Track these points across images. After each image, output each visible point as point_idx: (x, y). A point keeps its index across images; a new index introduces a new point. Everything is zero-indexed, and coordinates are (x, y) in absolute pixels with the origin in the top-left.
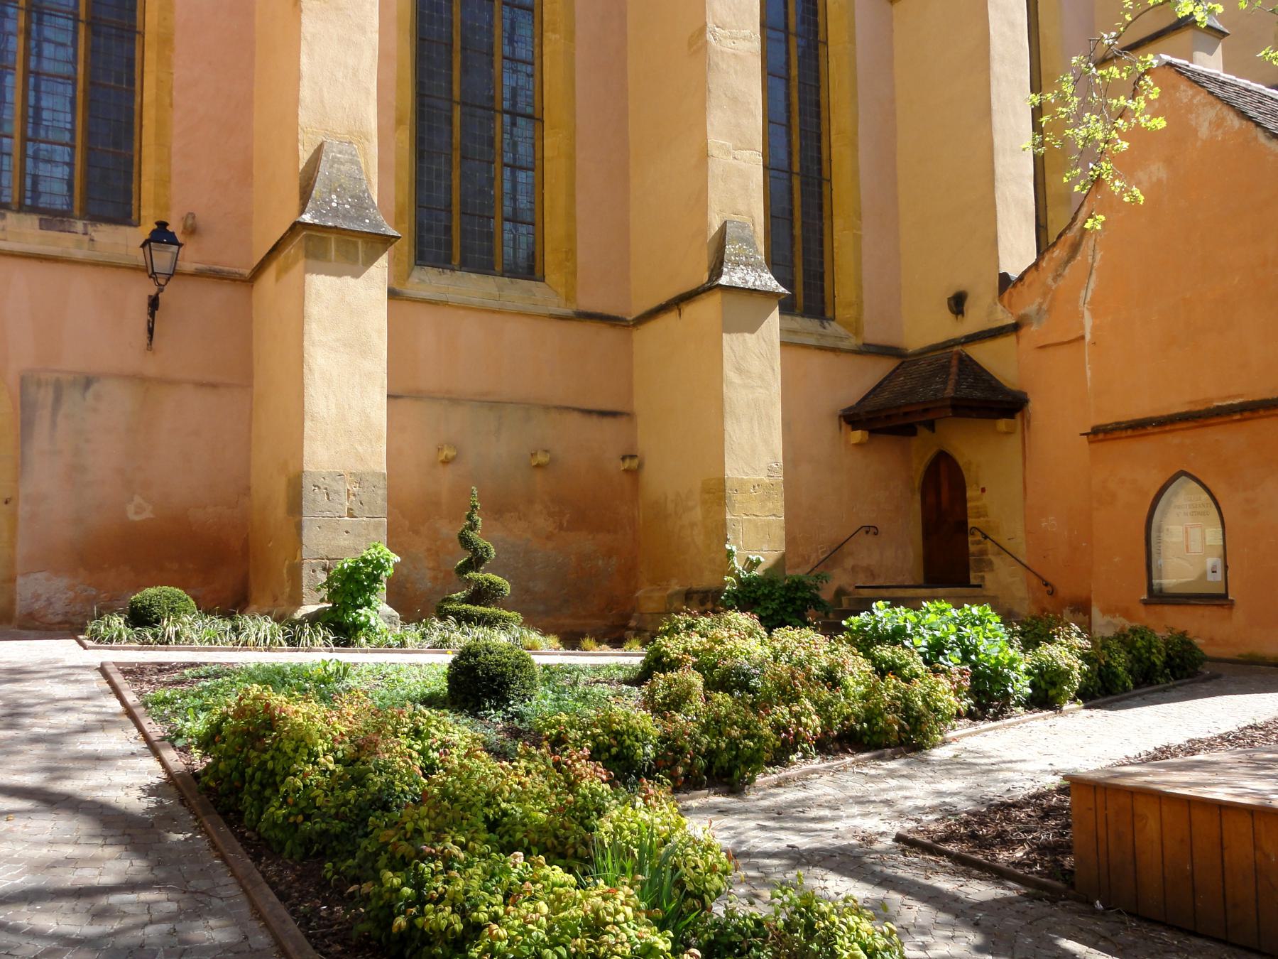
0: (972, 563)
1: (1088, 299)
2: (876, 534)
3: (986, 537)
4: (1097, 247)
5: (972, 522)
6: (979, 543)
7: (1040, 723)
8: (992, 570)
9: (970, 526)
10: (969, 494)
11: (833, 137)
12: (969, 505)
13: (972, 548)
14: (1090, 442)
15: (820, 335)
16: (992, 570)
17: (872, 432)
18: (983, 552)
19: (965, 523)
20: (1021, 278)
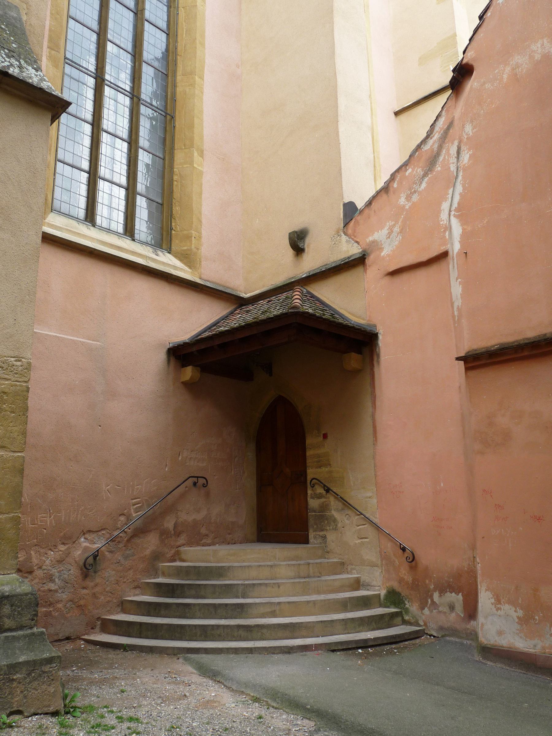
0: (311, 521)
1: (455, 205)
2: (204, 486)
3: (328, 490)
4: (463, 148)
5: (311, 473)
6: (320, 496)
7: (91, 106)
8: (336, 529)
9: (309, 478)
10: (309, 441)
11: (179, 78)
12: (309, 453)
13: (313, 503)
14: (467, 369)
15: (318, 587)
16: (336, 529)
17: (204, 369)
18: (324, 508)
19: (304, 474)
20: (369, 203)
